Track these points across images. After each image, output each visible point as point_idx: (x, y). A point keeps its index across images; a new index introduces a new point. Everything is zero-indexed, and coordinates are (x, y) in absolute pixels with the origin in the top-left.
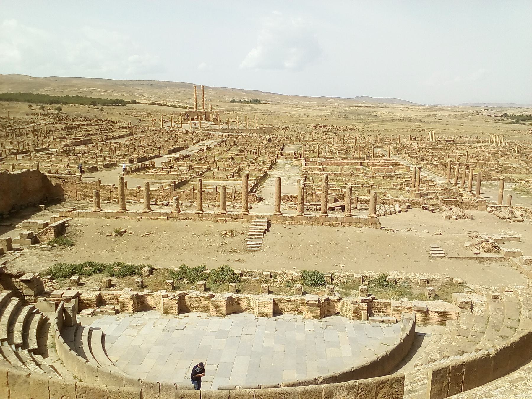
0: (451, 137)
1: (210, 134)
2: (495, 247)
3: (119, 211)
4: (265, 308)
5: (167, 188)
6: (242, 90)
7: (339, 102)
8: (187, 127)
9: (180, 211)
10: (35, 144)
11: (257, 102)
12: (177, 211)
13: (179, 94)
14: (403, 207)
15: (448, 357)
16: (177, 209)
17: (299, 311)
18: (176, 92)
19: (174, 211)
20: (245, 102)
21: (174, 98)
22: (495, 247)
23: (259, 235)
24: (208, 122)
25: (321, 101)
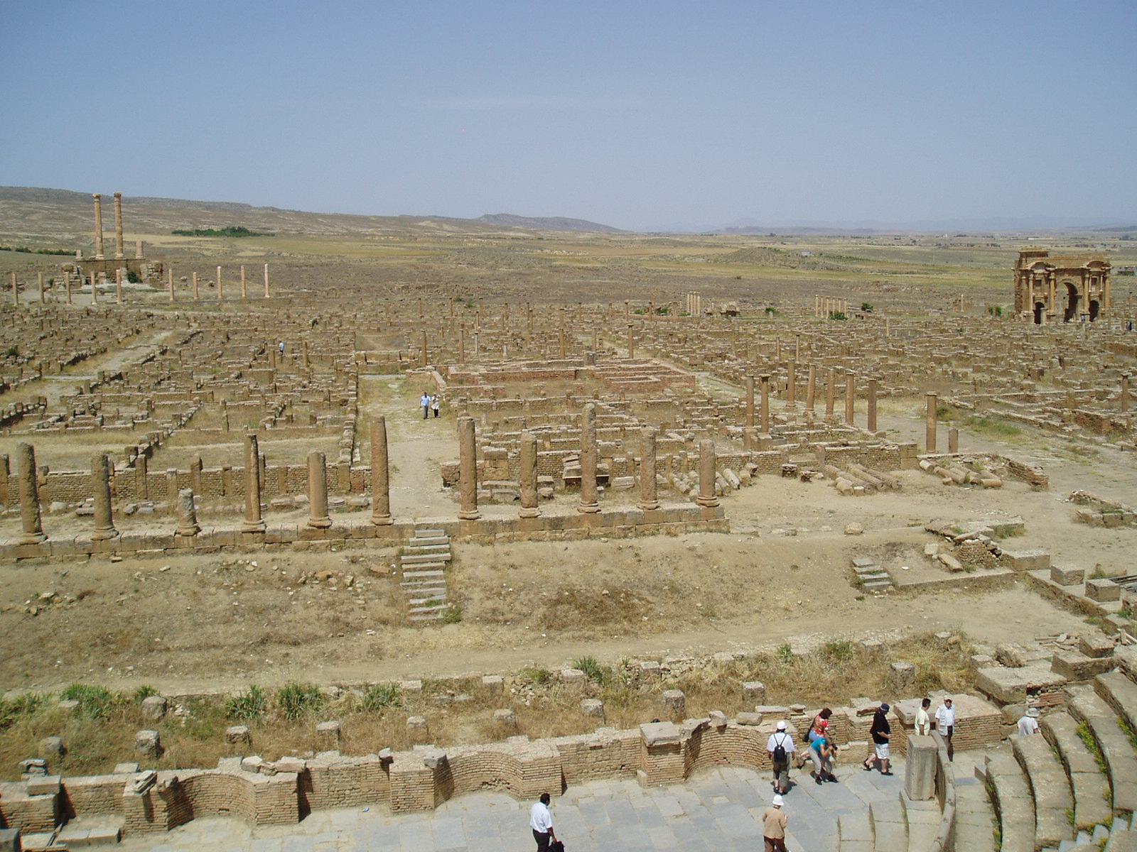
0: (734, 303)
1: (150, 316)
2: (993, 551)
3: (23, 540)
4: (541, 775)
5: (121, 466)
6: (199, 204)
7: (446, 227)
8: (84, 301)
9: (199, 530)
10: (950, 364)
11: (239, 232)
12: (191, 531)
13: (34, 217)
14: (745, 473)
15: (764, 820)
16: (190, 524)
17: (627, 770)
18: (27, 214)
19: (184, 531)
20: (209, 233)
21: (20, 229)
22: (993, 551)
23: (434, 577)
24: (136, 285)
25: (403, 226)
